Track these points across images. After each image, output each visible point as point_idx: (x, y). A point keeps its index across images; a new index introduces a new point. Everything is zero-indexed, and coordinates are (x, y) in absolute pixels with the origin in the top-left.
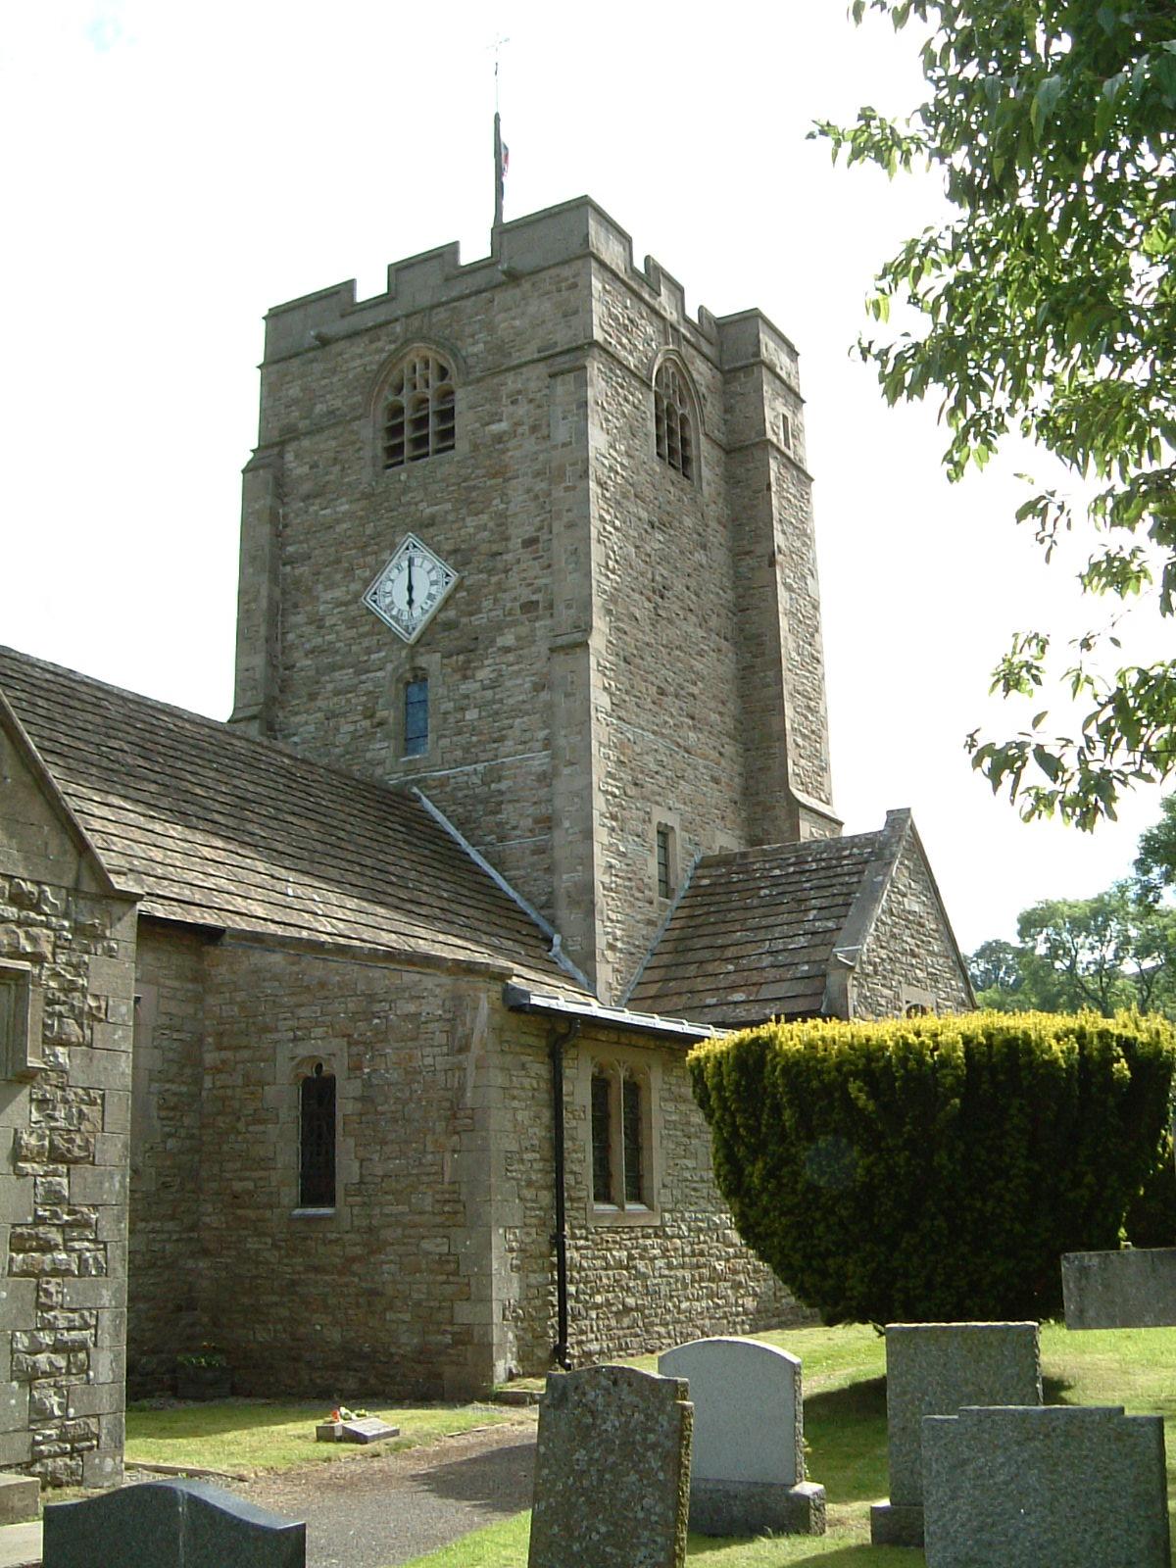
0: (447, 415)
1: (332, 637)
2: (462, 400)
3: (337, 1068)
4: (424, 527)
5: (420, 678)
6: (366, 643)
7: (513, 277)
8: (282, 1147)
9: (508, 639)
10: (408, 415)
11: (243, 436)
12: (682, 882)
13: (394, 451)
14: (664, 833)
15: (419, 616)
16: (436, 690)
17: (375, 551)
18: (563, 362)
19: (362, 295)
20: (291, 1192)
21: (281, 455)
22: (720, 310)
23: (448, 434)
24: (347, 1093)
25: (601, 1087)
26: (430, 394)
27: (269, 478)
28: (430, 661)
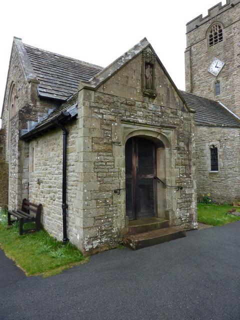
0: (221, 35)
1: (44, 259)
2: (224, 31)
3: (218, 146)
5: (218, 82)
6: (208, 77)
9: (235, 73)
10: (214, 36)
11: (184, 46)
13: (211, 43)
16: (222, 84)
17: (209, 61)
19: (223, 5)
20: (210, 168)
21: (191, 48)
24: (220, 152)
26: (217, 31)
27: (189, 51)
28: (220, 79)
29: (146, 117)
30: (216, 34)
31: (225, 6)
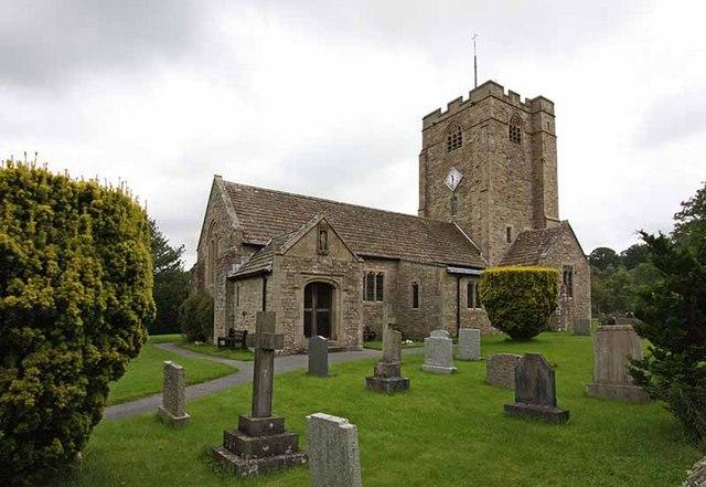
0: (460, 139)
4: (455, 165)
7: (473, 104)
8: (410, 297)
11: (419, 148)
12: (514, 236)
14: (509, 229)
15: (455, 186)
16: (459, 202)
17: (446, 172)
18: (485, 123)
19: (442, 112)
22: (531, 97)
23: (460, 143)
24: (420, 287)
25: (470, 286)
27: (424, 156)
28: (457, 195)
29: (319, 269)
30: (455, 136)
31: (466, 102)
